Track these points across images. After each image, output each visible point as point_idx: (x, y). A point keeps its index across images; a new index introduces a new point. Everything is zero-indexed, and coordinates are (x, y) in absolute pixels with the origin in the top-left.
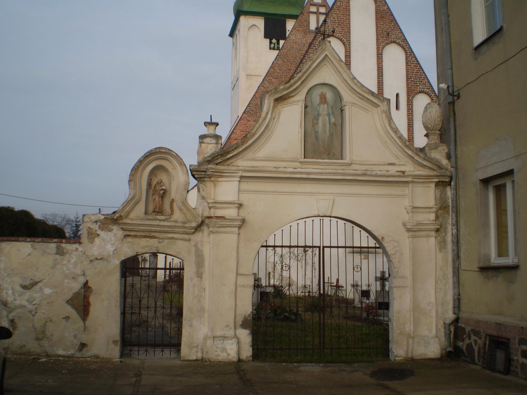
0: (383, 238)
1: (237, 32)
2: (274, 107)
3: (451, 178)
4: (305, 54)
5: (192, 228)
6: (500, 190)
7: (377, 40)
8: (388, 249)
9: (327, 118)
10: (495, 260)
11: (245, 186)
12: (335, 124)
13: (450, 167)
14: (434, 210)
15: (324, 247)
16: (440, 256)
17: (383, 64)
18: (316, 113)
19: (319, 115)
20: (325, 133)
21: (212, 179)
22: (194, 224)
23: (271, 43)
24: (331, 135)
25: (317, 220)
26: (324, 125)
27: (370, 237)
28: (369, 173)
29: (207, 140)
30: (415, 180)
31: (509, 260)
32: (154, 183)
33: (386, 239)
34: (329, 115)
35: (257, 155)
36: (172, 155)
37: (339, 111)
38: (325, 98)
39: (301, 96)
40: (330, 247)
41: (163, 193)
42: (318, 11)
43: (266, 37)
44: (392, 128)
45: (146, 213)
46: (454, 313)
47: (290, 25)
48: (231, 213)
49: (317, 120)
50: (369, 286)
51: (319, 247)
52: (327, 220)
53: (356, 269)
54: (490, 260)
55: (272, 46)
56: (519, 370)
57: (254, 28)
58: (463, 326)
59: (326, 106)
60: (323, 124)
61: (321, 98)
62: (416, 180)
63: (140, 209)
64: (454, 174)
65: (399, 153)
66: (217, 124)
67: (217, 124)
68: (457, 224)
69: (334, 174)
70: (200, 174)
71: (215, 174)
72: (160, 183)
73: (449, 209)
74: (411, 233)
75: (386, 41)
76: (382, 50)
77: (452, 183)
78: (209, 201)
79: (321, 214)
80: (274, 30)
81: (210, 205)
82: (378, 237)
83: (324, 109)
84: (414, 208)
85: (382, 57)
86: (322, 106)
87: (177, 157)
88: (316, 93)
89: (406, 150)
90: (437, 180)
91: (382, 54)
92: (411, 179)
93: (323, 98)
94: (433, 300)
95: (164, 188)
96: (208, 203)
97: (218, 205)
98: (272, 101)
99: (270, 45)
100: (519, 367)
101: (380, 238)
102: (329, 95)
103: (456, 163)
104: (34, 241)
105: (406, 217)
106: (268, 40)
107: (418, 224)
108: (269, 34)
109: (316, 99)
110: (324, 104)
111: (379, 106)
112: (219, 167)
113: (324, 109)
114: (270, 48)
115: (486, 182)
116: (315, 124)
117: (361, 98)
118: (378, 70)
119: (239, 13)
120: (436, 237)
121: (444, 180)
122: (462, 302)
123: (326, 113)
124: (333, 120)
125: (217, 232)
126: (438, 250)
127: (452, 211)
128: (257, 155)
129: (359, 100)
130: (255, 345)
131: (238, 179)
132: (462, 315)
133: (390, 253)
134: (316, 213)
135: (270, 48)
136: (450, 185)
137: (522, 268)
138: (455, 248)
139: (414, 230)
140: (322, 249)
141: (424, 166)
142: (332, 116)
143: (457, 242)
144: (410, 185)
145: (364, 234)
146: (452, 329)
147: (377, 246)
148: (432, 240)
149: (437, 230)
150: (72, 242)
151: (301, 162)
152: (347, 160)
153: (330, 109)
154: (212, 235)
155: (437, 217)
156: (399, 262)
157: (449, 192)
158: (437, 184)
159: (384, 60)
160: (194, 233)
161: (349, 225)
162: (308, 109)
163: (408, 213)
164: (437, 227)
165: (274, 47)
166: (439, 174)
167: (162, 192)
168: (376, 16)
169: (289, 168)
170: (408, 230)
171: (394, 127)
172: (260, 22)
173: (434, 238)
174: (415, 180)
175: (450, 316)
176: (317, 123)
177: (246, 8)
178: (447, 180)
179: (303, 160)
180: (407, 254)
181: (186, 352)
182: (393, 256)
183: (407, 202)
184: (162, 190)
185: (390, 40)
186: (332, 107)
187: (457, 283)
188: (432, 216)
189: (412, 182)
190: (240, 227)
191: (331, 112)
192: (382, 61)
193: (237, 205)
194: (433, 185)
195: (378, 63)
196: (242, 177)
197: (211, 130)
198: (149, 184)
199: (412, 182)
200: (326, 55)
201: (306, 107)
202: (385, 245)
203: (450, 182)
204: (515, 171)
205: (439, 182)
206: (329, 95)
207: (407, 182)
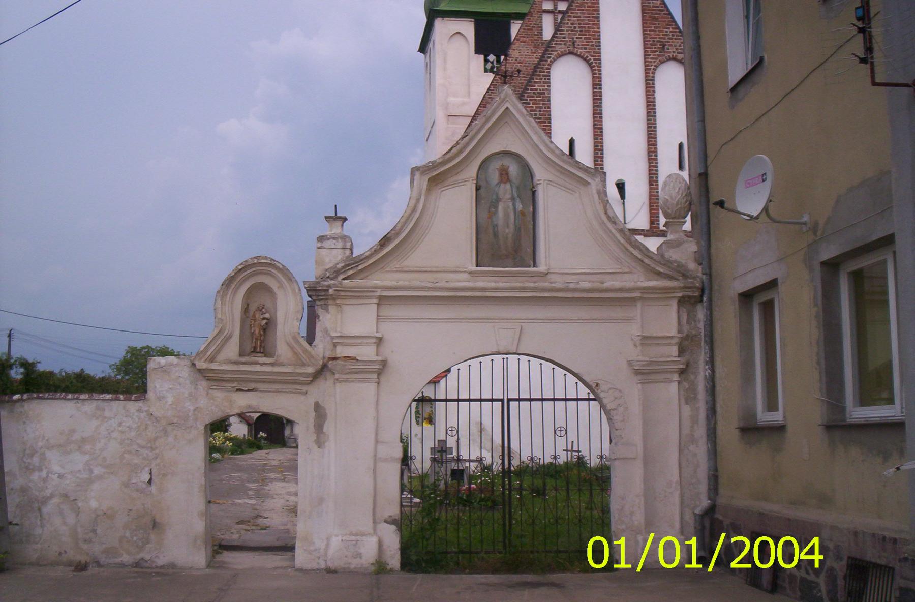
0: (597, 385)
1: (430, 45)
2: (429, 190)
3: (703, 290)
4: (527, 85)
5: (307, 375)
6: (768, 308)
7: (646, 56)
8: (605, 401)
9: (511, 204)
10: (764, 417)
11: (387, 311)
12: (523, 213)
13: (700, 274)
14: (676, 340)
15: (509, 400)
16: (687, 410)
17: (656, 95)
18: (494, 197)
19: (498, 200)
20: (508, 227)
21: (338, 302)
22: (310, 370)
23: (486, 61)
24: (518, 230)
25: (498, 359)
26: (507, 215)
27: (580, 384)
28: (572, 286)
29: (327, 244)
30: (645, 296)
31: (776, 418)
32: (253, 308)
33: (603, 387)
34: (513, 199)
35: (406, 263)
36: (277, 268)
37: (530, 193)
38: (507, 174)
39: (472, 171)
40: (519, 400)
41: (266, 324)
42: (556, 8)
43: (478, 51)
44: (608, 217)
45: (241, 354)
46: (709, 499)
47: (515, 28)
48: (367, 352)
49: (496, 208)
50: (555, 457)
51: (502, 400)
52: (513, 358)
53: (558, 433)
54: (754, 416)
55: (489, 66)
56: (787, 585)
57: (457, 40)
58: (721, 518)
59: (508, 186)
60: (505, 214)
61: (501, 175)
62: (647, 296)
63: (232, 350)
64: (706, 284)
65: (622, 255)
66: (345, 219)
67: (345, 219)
68: (711, 362)
69: (523, 289)
70: (319, 296)
71: (342, 294)
72: (261, 309)
73: (700, 340)
74: (640, 377)
75: (660, 58)
76: (653, 73)
77: (705, 299)
78: (333, 334)
79: (502, 349)
80: (492, 38)
81: (335, 341)
82: (591, 383)
83: (505, 191)
84: (644, 338)
85: (653, 84)
86: (502, 185)
87: (284, 271)
88: (495, 165)
89: (631, 249)
90: (680, 295)
91: (653, 80)
92: (639, 295)
93: (504, 175)
94: (675, 477)
95: (267, 316)
96: (332, 338)
97: (346, 341)
98: (426, 183)
99: (485, 65)
100: (787, 580)
101: (594, 386)
102: (514, 170)
103: (710, 267)
104: (77, 399)
105: (634, 354)
106: (482, 57)
107: (651, 363)
108: (481, 48)
109: (494, 177)
110: (505, 183)
111: (589, 183)
112: (357, 282)
113: (505, 191)
114: (486, 71)
115: (747, 297)
116: (492, 214)
117: (561, 173)
118: (647, 106)
119: (433, 14)
120: (679, 383)
121: (690, 294)
122: (721, 481)
123: (508, 196)
124: (519, 207)
125: (346, 381)
126: (683, 401)
127: (705, 341)
128: (406, 263)
129: (558, 174)
130: (404, 549)
131: (376, 301)
132: (721, 501)
133: (609, 407)
134: (495, 350)
135: (486, 71)
136: (701, 301)
137: (790, 428)
138: (710, 398)
139: (646, 373)
140: (506, 403)
141: (659, 274)
142: (518, 200)
143: (712, 390)
144: (639, 304)
145: (572, 379)
146: (707, 523)
147: (592, 396)
148: (674, 387)
149: (682, 372)
150: (133, 398)
151: (470, 273)
152: (542, 268)
153: (514, 190)
154: (338, 385)
155: (681, 352)
156: (623, 420)
157: (701, 313)
158: (682, 302)
159: (657, 89)
160: (312, 381)
161: (547, 366)
162: (482, 191)
163: (635, 345)
164: (681, 366)
165: (492, 68)
166: (682, 285)
167: (264, 322)
168: (643, 17)
169: (461, 281)
170: (638, 372)
171: (611, 215)
172: (468, 28)
173: (676, 383)
174: (645, 296)
175: (705, 503)
176: (496, 213)
177: (443, 7)
178: (697, 294)
179: (474, 268)
180: (635, 408)
181: (301, 557)
182: (614, 412)
183: (635, 330)
184: (264, 319)
185: (667, 55)
186: (518, 188)
187: (714, 453)
188: (674, 350)
189: (641, 298)
190: (379, 373)
191: (516, 195)
192: (654, 91)
193: (374, 340)
194: (674, 304)
195: (647, 95)
196: (381, 298)
197: (336, 229)
198: (246, 310)
199: (641, 298)
200: (507, 108)
201: (478, 188)
202: (602, 395)
203: (702, 296)
204: (780, 281)
205: (683, 297)
206: (514, 170)
207: (634, 299)
